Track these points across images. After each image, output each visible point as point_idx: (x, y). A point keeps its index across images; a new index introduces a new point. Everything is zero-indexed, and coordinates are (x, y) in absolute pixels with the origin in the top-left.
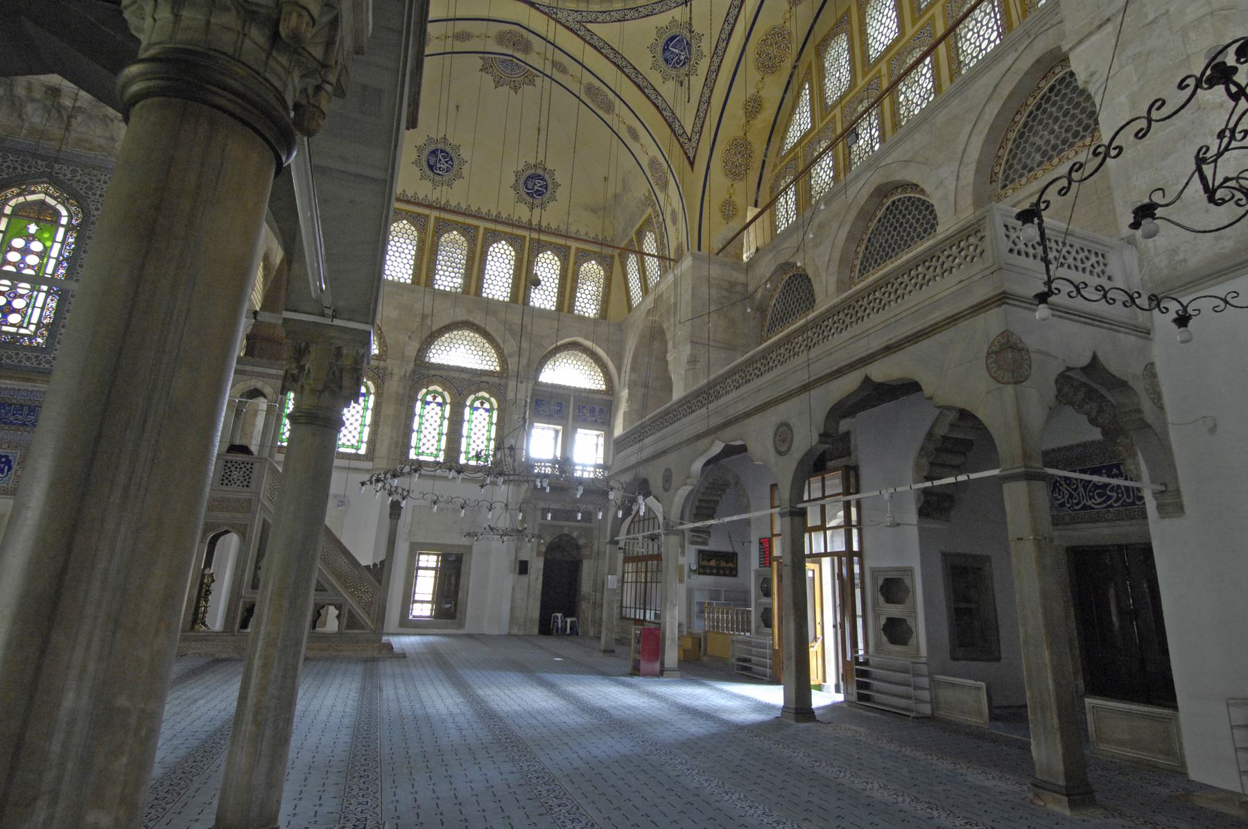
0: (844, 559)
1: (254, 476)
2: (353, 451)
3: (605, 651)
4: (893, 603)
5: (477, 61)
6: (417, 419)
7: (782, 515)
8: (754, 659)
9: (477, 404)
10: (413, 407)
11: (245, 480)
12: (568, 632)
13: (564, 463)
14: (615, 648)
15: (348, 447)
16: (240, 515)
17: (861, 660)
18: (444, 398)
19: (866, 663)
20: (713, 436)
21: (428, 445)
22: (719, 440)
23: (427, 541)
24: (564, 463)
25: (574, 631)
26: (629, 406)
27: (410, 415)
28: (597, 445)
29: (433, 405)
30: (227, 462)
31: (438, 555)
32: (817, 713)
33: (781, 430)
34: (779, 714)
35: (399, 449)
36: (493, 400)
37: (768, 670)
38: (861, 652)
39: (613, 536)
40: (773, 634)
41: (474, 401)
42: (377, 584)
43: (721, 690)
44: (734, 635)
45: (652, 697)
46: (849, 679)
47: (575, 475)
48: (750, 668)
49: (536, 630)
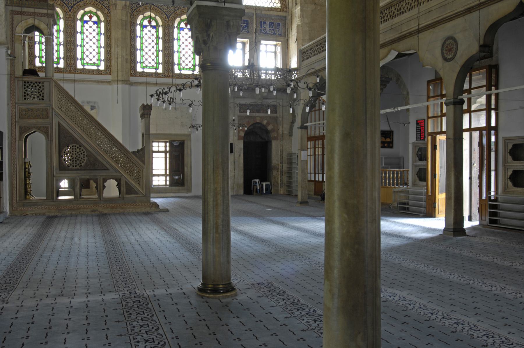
0: (484, 132)
1: (46, 92)
2: (95, 68)
3: (301, 203)
4: (517, 160)
6: (138, 40)
7: (447, 104)
8: (411, 202)
9: (86, 18)
10: (134, 31)
11: (40, 95)
12: (264, 192)
13: (253, 67)
14: (308, 200)
15: (91, 64)
16: (40, 120)
17: (492, 198)
18: (157, 22)
19: (496, 200)
20: (390, 47)
22: (394, 50)
23: (158, 132)
24: (253, 67)
25: (269, 191)
26: (301, 20)
27: (133, 37)
28: (275, 53)
29: (91, 24)
30: (25, 82)
31: (166, 142)
32: (466, 231)
33: (447, 42)
34: (441, 233)
35: (129, 64)
37: (423, 209)
38: (493, 194)
39: (302, 123)
40: (427, 185)
41: (179, 24)
42: (141, 163)
43: (395, 222)
44: (395, 188)
45: (318, 236)
46: (484, 212)
48: (408, 208)
49: (242, 192)
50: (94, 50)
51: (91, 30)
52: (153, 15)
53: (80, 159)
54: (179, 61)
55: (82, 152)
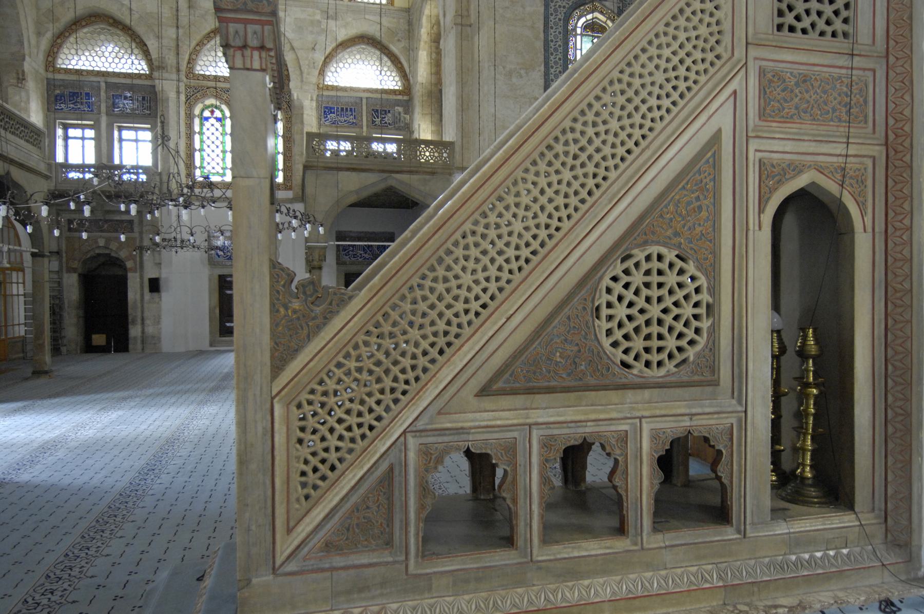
9: (207, 114)
21: (213, 164)
29: (212, 121)
36: (224, 107)
47: (145, 180)
50: (217, 138)
51: (213, 129)
53: (655, 343)
54: (202, 163)
55: (690, 334)
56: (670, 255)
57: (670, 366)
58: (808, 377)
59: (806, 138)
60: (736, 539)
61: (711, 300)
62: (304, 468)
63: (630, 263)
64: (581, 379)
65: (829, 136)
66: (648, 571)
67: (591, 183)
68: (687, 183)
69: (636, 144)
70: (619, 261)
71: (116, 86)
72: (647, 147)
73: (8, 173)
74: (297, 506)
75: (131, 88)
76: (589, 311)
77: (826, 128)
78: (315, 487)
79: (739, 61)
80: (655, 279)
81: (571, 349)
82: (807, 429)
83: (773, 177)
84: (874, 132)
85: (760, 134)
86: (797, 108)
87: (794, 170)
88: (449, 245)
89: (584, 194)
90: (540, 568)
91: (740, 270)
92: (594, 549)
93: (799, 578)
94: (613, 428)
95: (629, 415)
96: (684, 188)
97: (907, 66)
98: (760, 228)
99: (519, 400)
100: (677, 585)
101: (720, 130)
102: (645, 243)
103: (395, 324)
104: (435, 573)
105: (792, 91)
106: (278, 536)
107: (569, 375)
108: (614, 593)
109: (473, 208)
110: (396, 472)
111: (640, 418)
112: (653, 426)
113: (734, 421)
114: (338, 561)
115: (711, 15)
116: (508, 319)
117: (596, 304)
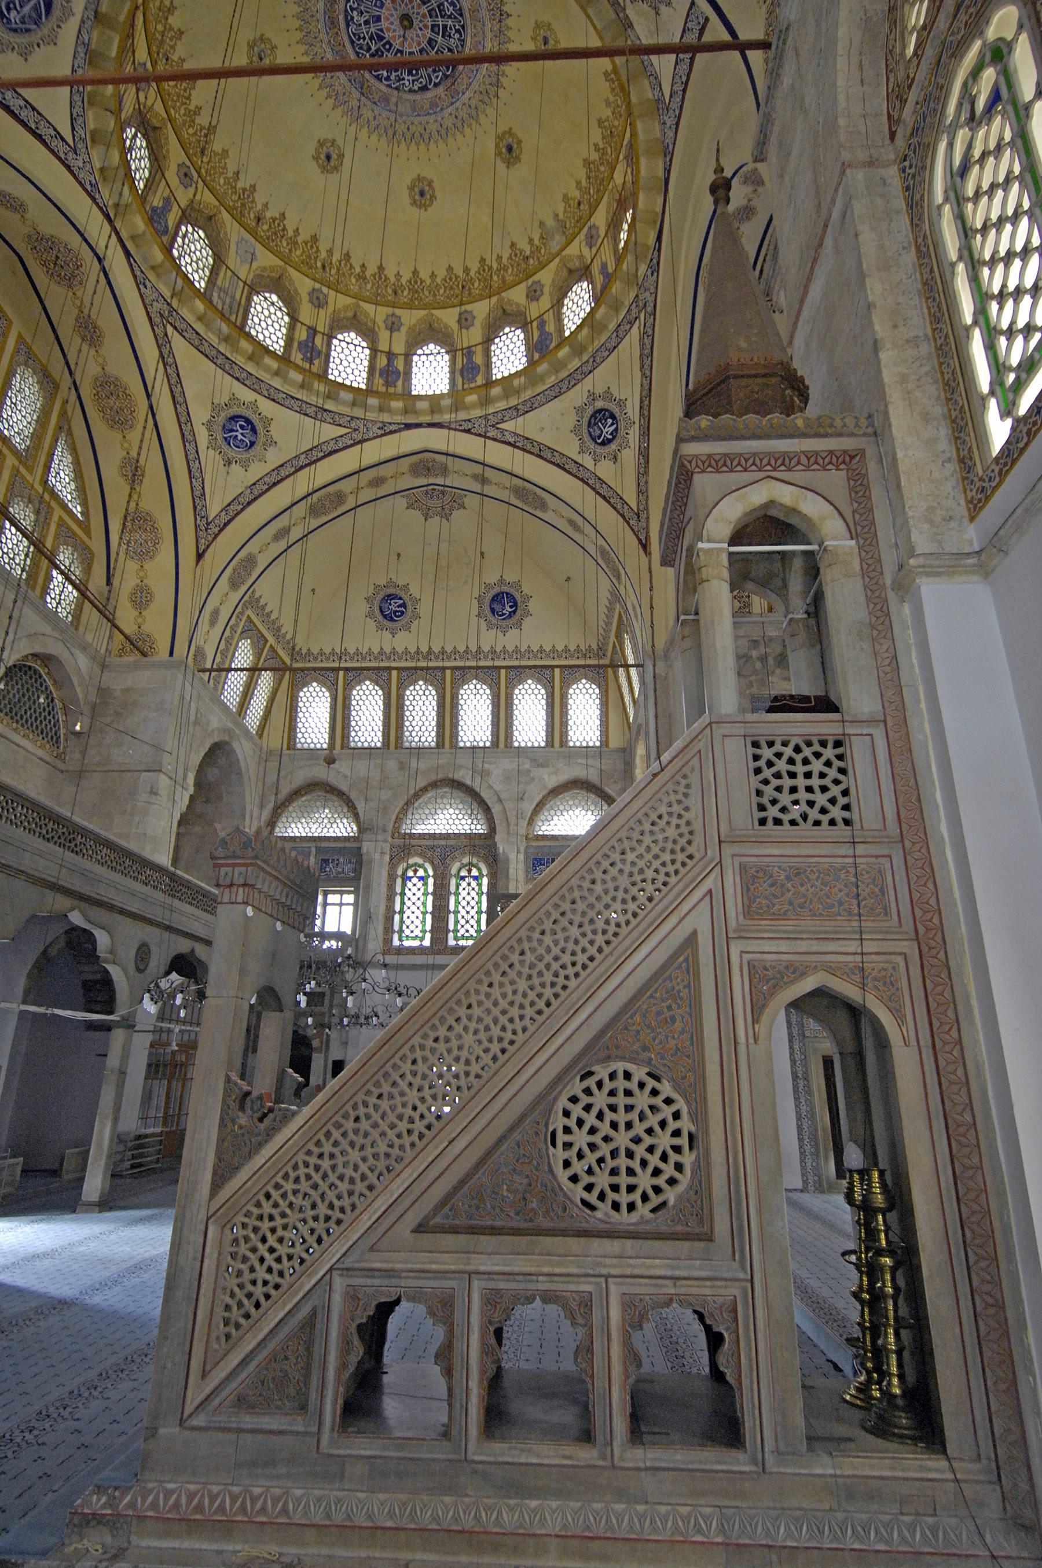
5: (401, 502)
9: (464, 873)
29: (415, 880)
51: (414, 890)
52: (475, 861)
55: (669, 1170)
56: (639, 1073)
57: (643, 1210)
58: (879, 1240)
59: (805, 936)
60: (750, 1472)
61: (693, 1129)
62: (229, 1300)
63: (591, 1082)
64: (531, 1220)
65: (836, 932)
66: (618, 1502)
67: (548, 992)
68: (656, 991)
69: (600, 950)
70: (578, 1078)
71: (326, 850)
72: (611, 953)
73: (193, 951)
74: (216, 1347)
75: (341, 851)
76: (542, 1137)
77: (833, 923)
78: (238, 1326)
79: (712, 860)
80: (621, 1100)
81: (521, 1181)
82: (887, 1317)
83: (768, 981)
84: (900, 925)
85: (743, 934)
86: (791, 903)
87: (794, 972)
88: (396, 1059)
89: (541, 1004)
90: (475, 1472)
91: (731, 1092)
92: (548, 1457)
93: (846, 1553)
94: (572, 1287)
95: (591, 1272)
96: (651, 996)
97: (924, 850)
98: (756, 1041)
99: (460, 1240)
100: (655, 1530)
101: (695, 933)
102: (608, 1058)
103: (336, 1144)
104: (349, 1456)
105: (782, 886)
106: (191, 1380)
107: (517, 1214)
108: (565, 1527)
109: (421, 1021)
110: (319, 1317)
111: (607, 1277)
112: (625, 1289)
113: (736, 1292)
114: (248, 1421)
115: (680, 816)
116: (450, 1143)
117: (551, 1129)
